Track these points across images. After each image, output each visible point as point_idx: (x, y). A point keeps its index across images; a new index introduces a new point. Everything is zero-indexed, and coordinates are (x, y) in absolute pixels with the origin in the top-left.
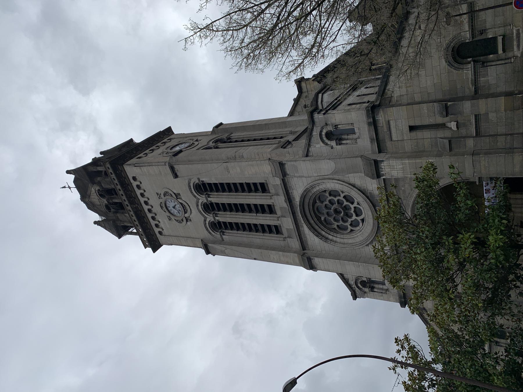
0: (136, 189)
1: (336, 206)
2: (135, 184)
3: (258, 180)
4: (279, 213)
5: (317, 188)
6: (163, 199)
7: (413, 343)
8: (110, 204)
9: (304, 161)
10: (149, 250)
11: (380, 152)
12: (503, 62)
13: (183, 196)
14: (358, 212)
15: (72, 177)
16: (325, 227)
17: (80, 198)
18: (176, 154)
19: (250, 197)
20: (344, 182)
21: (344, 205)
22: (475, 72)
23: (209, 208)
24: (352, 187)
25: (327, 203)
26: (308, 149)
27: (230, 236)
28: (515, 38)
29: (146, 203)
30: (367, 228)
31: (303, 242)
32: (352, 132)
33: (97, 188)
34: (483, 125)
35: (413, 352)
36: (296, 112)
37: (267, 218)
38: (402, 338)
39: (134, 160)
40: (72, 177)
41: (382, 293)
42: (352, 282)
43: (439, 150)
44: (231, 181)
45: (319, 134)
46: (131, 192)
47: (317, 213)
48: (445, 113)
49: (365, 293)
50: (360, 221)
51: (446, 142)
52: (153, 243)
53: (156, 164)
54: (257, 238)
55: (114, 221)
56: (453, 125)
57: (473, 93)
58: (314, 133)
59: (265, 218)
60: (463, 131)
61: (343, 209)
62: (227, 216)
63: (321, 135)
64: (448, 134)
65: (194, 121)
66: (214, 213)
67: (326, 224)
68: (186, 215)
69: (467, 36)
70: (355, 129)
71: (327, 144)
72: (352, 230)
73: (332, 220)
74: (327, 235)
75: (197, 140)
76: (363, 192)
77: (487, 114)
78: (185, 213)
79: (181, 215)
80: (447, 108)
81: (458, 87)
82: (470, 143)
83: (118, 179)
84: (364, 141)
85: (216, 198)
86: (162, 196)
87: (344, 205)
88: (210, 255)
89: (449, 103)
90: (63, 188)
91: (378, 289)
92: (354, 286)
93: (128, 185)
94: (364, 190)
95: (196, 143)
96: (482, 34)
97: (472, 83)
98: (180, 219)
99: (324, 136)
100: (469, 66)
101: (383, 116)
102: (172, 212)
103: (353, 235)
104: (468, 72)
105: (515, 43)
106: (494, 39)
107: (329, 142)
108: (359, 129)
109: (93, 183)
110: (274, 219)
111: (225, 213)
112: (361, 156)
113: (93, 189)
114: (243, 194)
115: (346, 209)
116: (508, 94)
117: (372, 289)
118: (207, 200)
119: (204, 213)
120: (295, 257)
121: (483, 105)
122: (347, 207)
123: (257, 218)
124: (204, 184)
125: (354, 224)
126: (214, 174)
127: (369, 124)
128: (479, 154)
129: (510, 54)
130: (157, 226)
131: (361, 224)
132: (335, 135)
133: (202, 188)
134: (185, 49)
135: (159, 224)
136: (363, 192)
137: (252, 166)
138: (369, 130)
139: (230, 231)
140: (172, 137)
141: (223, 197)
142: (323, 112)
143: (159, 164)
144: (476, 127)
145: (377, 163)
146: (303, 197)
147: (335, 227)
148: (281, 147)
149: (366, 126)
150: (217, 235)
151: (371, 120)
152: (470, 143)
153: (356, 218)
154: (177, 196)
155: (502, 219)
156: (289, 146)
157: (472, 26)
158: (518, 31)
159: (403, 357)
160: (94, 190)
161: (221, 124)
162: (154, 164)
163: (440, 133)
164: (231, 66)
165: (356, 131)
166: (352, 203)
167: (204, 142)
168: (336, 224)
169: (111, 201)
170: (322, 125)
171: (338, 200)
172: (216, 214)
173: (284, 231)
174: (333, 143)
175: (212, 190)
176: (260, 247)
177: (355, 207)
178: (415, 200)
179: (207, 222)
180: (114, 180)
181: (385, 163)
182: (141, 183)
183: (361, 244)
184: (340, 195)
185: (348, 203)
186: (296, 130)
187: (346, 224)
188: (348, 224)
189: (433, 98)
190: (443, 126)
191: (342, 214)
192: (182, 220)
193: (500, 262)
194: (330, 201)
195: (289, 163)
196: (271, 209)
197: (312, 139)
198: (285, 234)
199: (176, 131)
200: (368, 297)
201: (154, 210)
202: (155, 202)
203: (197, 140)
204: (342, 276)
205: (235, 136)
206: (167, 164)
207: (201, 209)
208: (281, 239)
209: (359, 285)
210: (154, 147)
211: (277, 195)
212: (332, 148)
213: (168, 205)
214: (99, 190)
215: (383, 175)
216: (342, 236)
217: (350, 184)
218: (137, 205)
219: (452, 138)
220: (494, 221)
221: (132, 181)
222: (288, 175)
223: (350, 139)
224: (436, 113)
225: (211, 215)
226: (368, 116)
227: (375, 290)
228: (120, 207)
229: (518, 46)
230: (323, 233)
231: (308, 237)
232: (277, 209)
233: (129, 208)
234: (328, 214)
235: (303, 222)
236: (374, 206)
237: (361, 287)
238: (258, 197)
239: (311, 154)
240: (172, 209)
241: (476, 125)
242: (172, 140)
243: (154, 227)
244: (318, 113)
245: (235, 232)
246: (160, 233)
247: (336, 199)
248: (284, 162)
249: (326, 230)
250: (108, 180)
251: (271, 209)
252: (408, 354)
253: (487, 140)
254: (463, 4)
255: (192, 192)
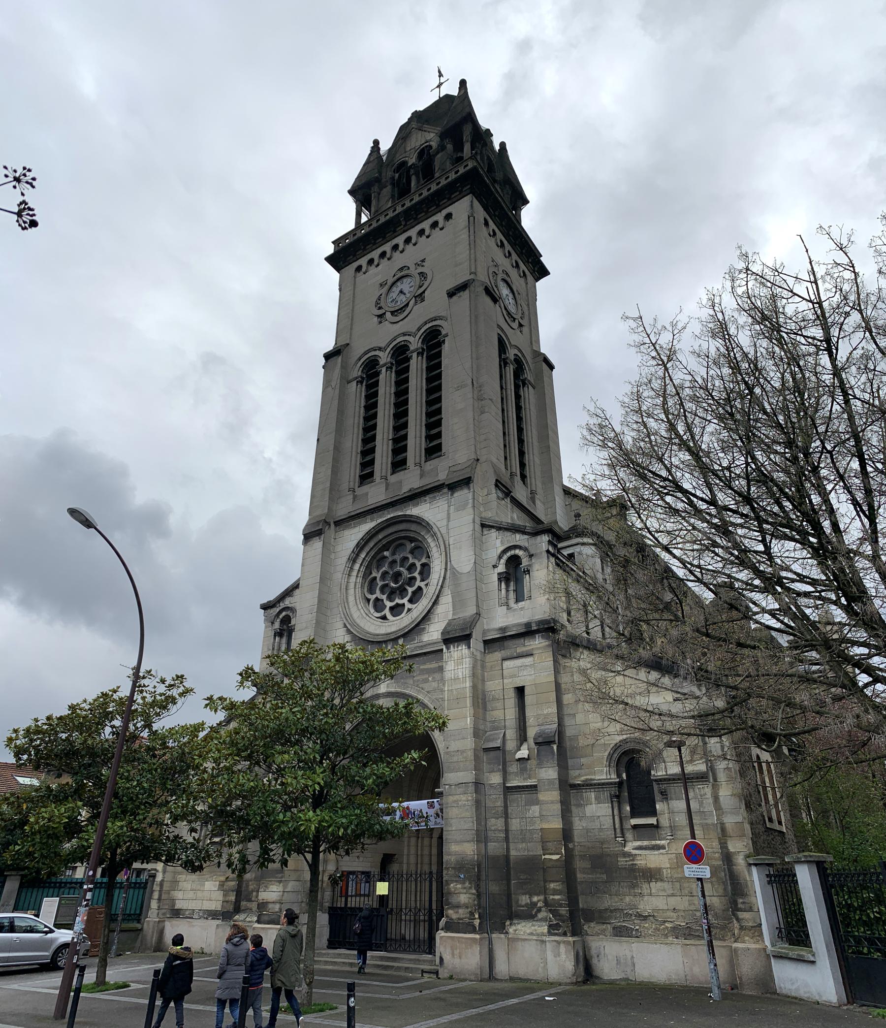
0: (379, 251)
1: (406, 574)
2: (440, 217)
3: (446, 440)
4: (393, 479)
5: (432, 544)
6: (413, 271)
7: (180, 701)
8: (408, 171)
9: (474, 522)
10: (330, 250)
11: (486, 642)
12: (617, 825)
13: (420, 306)
14: (396, 610)
15: (455, 92)
16: (373, 557)
17: (418, 109)
18: (488, 291)
19: (418, 427)
20: (442, 587)
21: (408, 588)
22: (603, 784)
23: (401, 353)
24: (433, 600)
25: (411, 561)
26: (492, 527)
27: (356, 394)
28: (653, 842)
29: (408, 240)
30: (374, 626)
31: (348, 521)
32: (519, 598)
33: (434, 144)
34: (523, 797)
35: (165, 703)
36: (570, 500)
37: (384, 458)
38: (187, 684)
39: (481, 213)
40: (455, 92)
41: (273, 649)
42: (287, 602)
43: (486, 732)
44: (444, 393)
45: (518, 543)
46: (427, 212)
47: (395, 544)
48: (540, 740)
49: (273, 623)
50: (383, 613)
51: (498, 743)
52: (343, 255)
53: (473, 256)
54: (353, 442)
55: (378, 180)
56: (523, 753)
57: (572, 782)
58: (518, 536)
59: (385, 454)
60: (513, 768)
61: (400, 586)
62: (388, 388)
63: (515, 547)
64: (511, 745)
65: (560, 315)
66: (392, 364)
67: (377, 560)
68: (388, 315)
69: (659, 772)
70: (523, 603)
71: (500, 557)
72: (368, 600)
73: (384, 569)
74: (359, 561)
75: (521, 325)
76: (426, 618)
77: (537, 802)
78: (392, 313)
79: (389, 306)
80: (549, 743)
81: (582, 760)
82: (496, 779)
83: (412, 206)
84: (503, 617)
85: (417, 366)
86: (420, 270)
87: (408, 588)
88: (324, 361)
89: (555, 747)
90: (439, 72)
91: (280, 643)
92: (282, 605)
93: (438, 206)
94: (429, 620)
95: (515, 325)
96: (661, 793)
97: (587, 780)
98: (382, 304)
99: (512, 552)
100: (614, 776)
101: (541, 645)
102: (394, 289)
103: (361, 604)
104: (604, 774)
105: (645, 843)
106: (653, 813)
107: (503, 561)
108: (522, 609)
109: (443, 136)
110: (384, 471)
111: (393, 383)
112: (478, 614)
113: (432, 135)
114: (424, 415)
115: (401, 592)
116: (567, 834)
117: (279, 634)
118: (413, 352)
119: (391, 346)
120: (322, 511)
121: (551, 797)
122: (404, 594)
123: (385, 440)
124: (440, 344)
125: (378, 605)
126: (455, 362)
127: (528, 625)
128: (477, 791)
129: (629, 835)
130: (371, 262)
131: (379, 615)
132: (514, 572)
133: (433, 340)
134: (626, 318)
135: (373, 266)
136: (426, 618)
137: (470, 427)
138: (518, 625)
139: (363, 394)
140: (530, 278)
141: (419, 379)
142: (551, 549)
143: (473, 261)
144: (519, 787)
145: (465, 638)
146: (418, 521)
147: (374, 575)
148: (497, 480)
149: (525, 620)
150: (357, 372)
151: (534, 628)
152: (496, 779)
153: (388, 608)
154: (420, 298)
155: (345, 829)
156: (500, 495)
157: (674, 780)
158: (663, 847)
159: (155, 687)
160: (430, 137)
161: (551, 367)
162: (472, 251)
163: (511, 734)
164: (595, 400)
165: (520, 604)
166: (411, 601)
167: (515, 338)
168: (379, 576)
169: (412, 171)
170: (530, 549)
171: (414, 578)
172: (391, 368)
173: (365, 488)
174: (501, 568)
175: (429, 359)
176: (337, 448)
177: (403, 605)
178: (412, 697)
179: (377, 353)
180: (446, 178)
181: (467, 651)
182: (441, 229)
183: (347, 616)
184: (422, 580)
185: (410, 594)
186: (538, 502)
187: (378, 591)
188: (378, 594)
189: (568, 721)
190: (522, 738)
191: (393, 585)
192: (380, 308)
193: (279, 827)
194: (414, 565)
195: (470, 495)
196: (399, 464)
197: (509, 534)
198: (360, 491)
199: (542, 285)
200: (266, 627)
201: (397, 255)
202: (408, 257)
203: (521, 325)
204: (296, 586)
205: (529, 395)
206: (472, 277)
207: (398, 340)
208: (352, 483)
209: (284, 614)
210: (508, 247)
211: (422, 476)
212: (495, 567)
213: (405, 280)
214: (431, 147)
215: (448, 648)
216: (359, 585)
217: (438, 597)
218: (403, 223)
219: (504, 752)
220: (345, 817)
221: (444, 212)
222: (452, 495)
223: (507, 596)
224: (542, 727)
225: (389, 359)
226: (540, 622)
227: (277, 639)
228: (403, 191)
229: (640, 848)
230: (363, 555)
231: (356, 530)
232: (400, 475)
233: (399, 209)
234: (394, 562)
235: (379, 521)
236: (404, 636)
237: (281, 617)
238: (418, 442)
239: (485, 532)
240: (399, 289)
241: (523, 787)
242: (523, 280)
243: (369, 257)
244: (549, 541)
245: (363, 403)
246: (359, 269)
247: (416, 574)
248: (471, 485)
249: (368, 559)
250: (448, 165)
251: (399, 464)
252: (161, 695)
253: (500, 803)
254: (707, 765)
255: (426, 323)
